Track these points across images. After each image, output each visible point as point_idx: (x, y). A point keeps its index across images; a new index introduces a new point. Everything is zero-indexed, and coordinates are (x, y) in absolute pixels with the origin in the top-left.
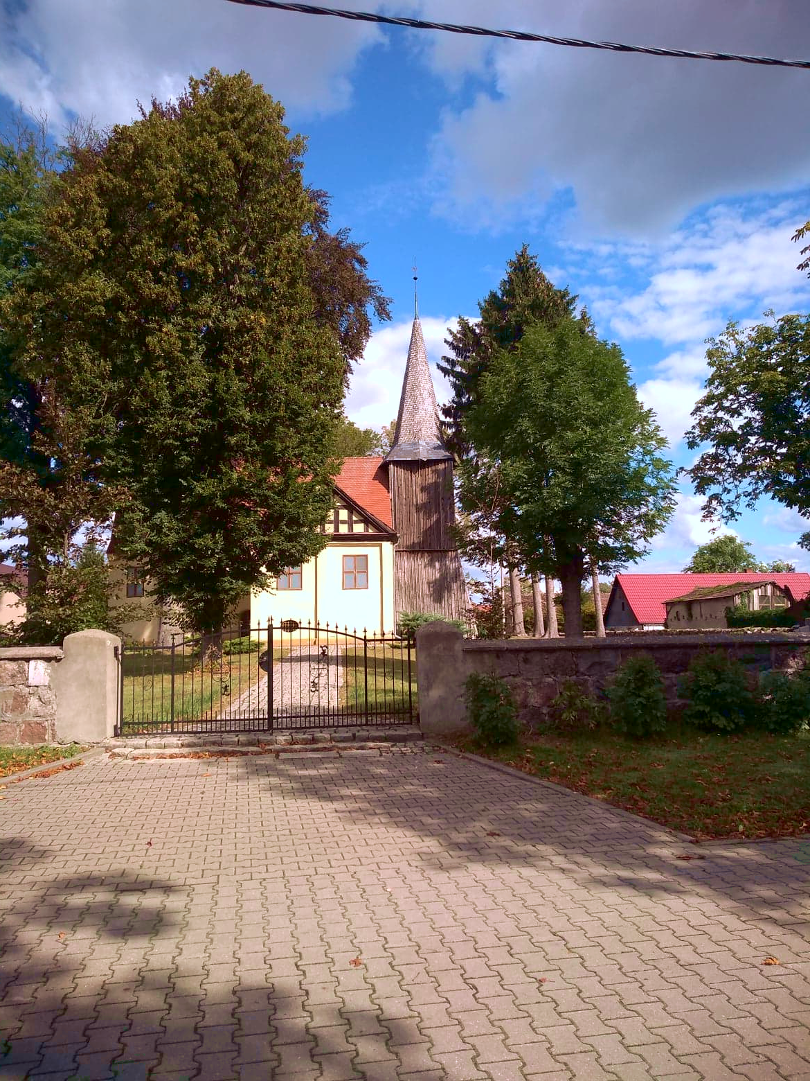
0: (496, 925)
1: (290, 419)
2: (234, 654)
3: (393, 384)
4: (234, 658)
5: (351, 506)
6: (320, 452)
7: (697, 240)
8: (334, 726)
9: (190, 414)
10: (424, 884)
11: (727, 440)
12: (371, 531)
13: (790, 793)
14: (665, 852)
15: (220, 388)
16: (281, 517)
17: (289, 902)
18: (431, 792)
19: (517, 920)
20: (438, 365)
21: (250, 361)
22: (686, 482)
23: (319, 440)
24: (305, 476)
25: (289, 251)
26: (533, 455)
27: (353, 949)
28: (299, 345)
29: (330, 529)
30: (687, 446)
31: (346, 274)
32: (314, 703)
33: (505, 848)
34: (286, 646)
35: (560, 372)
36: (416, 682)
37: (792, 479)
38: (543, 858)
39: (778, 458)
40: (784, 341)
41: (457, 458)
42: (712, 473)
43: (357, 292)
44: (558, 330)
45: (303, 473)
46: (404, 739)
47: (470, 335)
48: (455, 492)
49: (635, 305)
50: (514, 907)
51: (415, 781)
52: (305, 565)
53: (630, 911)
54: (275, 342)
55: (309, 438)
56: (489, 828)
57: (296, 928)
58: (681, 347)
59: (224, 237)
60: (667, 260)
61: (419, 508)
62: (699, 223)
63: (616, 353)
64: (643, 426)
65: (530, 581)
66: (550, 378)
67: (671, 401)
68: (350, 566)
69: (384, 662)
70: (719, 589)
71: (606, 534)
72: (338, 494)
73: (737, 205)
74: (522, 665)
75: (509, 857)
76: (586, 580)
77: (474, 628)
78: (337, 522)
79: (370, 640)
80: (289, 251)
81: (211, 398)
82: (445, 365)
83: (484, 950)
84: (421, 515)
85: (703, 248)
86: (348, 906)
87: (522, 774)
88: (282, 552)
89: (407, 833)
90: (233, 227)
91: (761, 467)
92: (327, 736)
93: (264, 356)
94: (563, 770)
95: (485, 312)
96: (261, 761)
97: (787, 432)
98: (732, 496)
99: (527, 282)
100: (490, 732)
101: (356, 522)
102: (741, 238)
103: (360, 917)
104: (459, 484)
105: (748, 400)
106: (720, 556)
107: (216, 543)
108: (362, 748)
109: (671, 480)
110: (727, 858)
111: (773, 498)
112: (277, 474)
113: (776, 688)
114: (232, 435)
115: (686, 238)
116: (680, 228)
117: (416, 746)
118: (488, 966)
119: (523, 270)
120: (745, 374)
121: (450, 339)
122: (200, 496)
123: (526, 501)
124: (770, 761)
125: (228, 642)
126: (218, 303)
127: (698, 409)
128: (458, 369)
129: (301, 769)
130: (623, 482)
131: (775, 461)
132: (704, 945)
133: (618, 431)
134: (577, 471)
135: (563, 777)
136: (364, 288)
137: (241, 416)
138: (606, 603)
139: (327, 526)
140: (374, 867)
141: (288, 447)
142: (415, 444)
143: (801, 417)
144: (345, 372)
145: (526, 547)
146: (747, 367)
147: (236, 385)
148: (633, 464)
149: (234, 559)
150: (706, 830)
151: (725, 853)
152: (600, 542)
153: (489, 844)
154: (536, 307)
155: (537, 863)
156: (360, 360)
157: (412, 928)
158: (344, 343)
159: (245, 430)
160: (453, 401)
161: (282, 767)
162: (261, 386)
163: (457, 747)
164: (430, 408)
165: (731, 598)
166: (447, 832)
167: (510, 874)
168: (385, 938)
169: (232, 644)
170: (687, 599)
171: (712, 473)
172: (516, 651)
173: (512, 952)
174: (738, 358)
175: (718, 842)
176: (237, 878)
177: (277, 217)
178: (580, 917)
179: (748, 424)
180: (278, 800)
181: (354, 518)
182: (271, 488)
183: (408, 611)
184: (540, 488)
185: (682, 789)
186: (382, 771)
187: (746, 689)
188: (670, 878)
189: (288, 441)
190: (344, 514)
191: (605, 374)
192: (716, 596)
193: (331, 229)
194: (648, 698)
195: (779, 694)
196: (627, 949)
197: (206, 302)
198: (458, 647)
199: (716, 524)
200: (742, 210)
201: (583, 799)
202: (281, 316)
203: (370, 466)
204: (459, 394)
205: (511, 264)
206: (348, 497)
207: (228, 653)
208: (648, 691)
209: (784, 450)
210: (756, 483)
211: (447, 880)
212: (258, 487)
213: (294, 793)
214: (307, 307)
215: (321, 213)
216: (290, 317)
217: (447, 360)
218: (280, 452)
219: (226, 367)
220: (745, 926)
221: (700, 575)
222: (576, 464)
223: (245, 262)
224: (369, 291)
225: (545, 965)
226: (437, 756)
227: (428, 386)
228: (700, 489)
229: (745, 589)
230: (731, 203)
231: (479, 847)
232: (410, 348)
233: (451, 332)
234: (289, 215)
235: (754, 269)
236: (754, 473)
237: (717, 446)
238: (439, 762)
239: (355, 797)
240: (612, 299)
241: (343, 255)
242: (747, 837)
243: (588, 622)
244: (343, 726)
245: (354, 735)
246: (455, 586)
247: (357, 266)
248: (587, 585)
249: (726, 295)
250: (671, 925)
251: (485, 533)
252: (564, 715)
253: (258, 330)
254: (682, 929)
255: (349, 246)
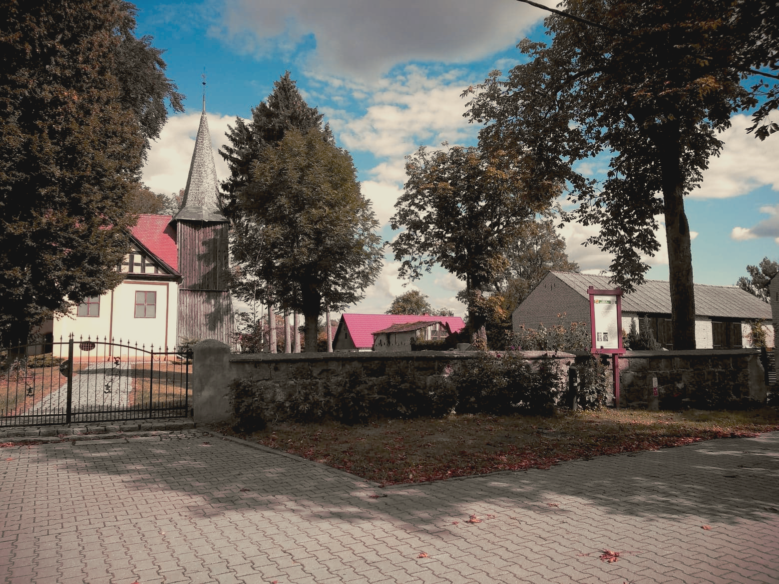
0: (243, 550)
1: (95, 178)
2: (38, 367)
3: (182, 160)
4: (39, 371)
5: (144, 252)
6: (120, 207)
7: (397, 86)
8: (123, 420)
9: (5, 166)
10: (191, 527)
11: (416, 225)
12: (160, 273)
13: (442, 453)
14: (362, 494)
15: (35, 148)
16: (84, 256)
17: (81, 548)
18: (199, 465)
19: (259, 545)
20: (219, 151)
21: (62, 128)
22: (389, 252)
23: (120, 198)
24: (107, 225)
25: (101, 46)
26: (288, 223)
27: (133, 576)
28: (105, 121)
29: (125, 269)
30: (391, 227)
31: (148, 72)
32: (108, 403)
33: (253, 499)
34: (85, 361)
35: (309, 166)
36: (192, 388)
37: (453, 255)
38: (280, 504)
39: (446, 240)
40: (453, 163)
41: (232, 222)
42: (406, 247)
43: (156, 87)
44: (309, 136)
45: (104, 222)
46: (180, 428)
47: (244, 132)
48: (230, 246)
49: (357, 125)
50: (257, 537)
51: (188, 458)
52: (102, 297)
53: (336, 533)
54: (85, 116)
55: (111, 195)
56: (242, 486)
57: (86, 566)
58: (386, 159)
59: (42, 24)
60: (378, 98)
61: (200, 258)
62: (398, 73)
63: (347, 157)
64: (363, 211)
65: (283, 315)
66: (302, 170)
67: (382, 195)
68: (142, 300)
69: (167, 374)
70: (407, 325)
71: (336, 283)
72: (133, 242)
73: (424, 67)
74: (273, 372)
75: (254, 505)
76: (322, 315)
77: (239, 347)
78: (132, 264)
79: (155, 354)
80: (101, 46)
81: (25, 155)
82: (225, 151)
83: (234, 567)
84: (202, 262)
85: (401, 93)
86: (130, 547)
87: (268, 449)
88: (83, 285)
89: (179, 493)
90: (51, 18)
91: (435, 245)
92: (117, 427)
93: (75, 126)
94: (297, 444)
95: (256, 116)
96: (59, 447)
97: (452, 223)
98: (417, 263)
99: (288, 99)
100: (247, 420)
101: (148, 265)
102: (426, 90)
103: (139, 554)
104: (233, 240)
105: (430, 200)
106: (409, 304)
107: (24, 274)
108: (146, 435)
109: (380, 249)
110: (401, 496)
111: (442, 266)
112: (81, 221)
113: (436, 387)
114: (43, 187)
115: (391, 84)
116: (386, 77)
117: (190, 433)
118: (236, 577)
119: (285, 90)
120: (429, 183)
121: (229, 133)
122: (11, 235)
123: (281, 256)
124: (431, 434)
125: (32, 358)
126: (35, 78)
127: (399, 203)
128: (235, 156)
129: (94, 452)
130: (349, 247)
131: (444, 241)
132: (382, 549)
133: (347, 212)
134: (318, 237)
135: (296, 449)
136: (162, 84)
137: (52, 173)
138: (335, 333)
139: (123, 267)
140: (153, 518)
141: (93, 201)
142: (198, 208)
143: (461, 214)
144: (144, 147)
145: (281, 289)
146: (430, 178)
147: (49, 147)
148: (356, 237)
149: (40, 289)
150: (389, 479)
151: (401, 493)
152: (332, 289)
153: (242, 497)
154: (294, 118)
155: (275, 507)
156: (157, 139)
157: (180, 558)
158: (143, 123)
159: (55, 184)
160: (230, 179)
161: (78, 451)
162: (72, 149)
163: (221, 432)
164: (212, 182)
165: (414, 331)
166: (210, 491)
167: (254, 516)
168: (159, 566)
169: (36, 359)
170: (387, 332)
171: (406, 247)
172: (269, 362)
173: (254, 566)
174: (425, 171)
175: (396, 486)
176: (35, 534)
177: (90, 17)
178: (303, 539)
179: (429, 216)
180: (74, 476)
181: (147, 262)
182: (76, 232)
183: (188, 336)
184: (292, 247)
185: (376, 454)
186: (161, 451)
187: (419, 388)
188: (364, 510)
189: (93, 196)
190: (138, 258)
191: (340, 171)
192: (405, 330)
193: (138, 33)
194: (358, 392)
195: (439, 391)
196: (333, 557)
197: (23, 75)
198: (226, 359)
199: (407, 281)
200: (427, 71)
201: (310, 463)
202: (91, 96)
203: (161, 222)
204: (235, 174)
205: (277, 84)
206: (143, 245)
207: (31, 367)
208: (358, 389)
209: (449, 235)
210: (432, 255)
211: (209, 523)
212: (65, 231)
213: (87, 470)
214: (115, 92)
215: (129, 21)
216: (99, 98)
217: (227, 148)
218: (85, 204)
219: (41, 131)
220: (409, 536)
221: (396, 316)
222: (318, 232)
223: (61, 48)
224: (166, 87)
225: (277, 572)
226: (205, 439)
227: (211, 166)
228: (398, 257)
229: (423, 326)
230: (421, 65)
231: (233, 499)
232: (198, 135)
233: (230, 128)
234: (102, 17)
235: (434, 112)
236: (431, 249)
237: (410, 229)
238: (207, 443)
239: (139, 471)
240: (342, 119)
241: (145, 56)
242: (414, 482)
243: (322, 347)
244: (130, 419)
245: (140, 426)
246: (226, 318)
247: (157, 66)
248: (322, 319)
249: (416, 127)
250: (362, 539)
251: (250, 278)
252: (301, 407)
253: (71, 104)
254: (369, 541)
255: (151, 50)
